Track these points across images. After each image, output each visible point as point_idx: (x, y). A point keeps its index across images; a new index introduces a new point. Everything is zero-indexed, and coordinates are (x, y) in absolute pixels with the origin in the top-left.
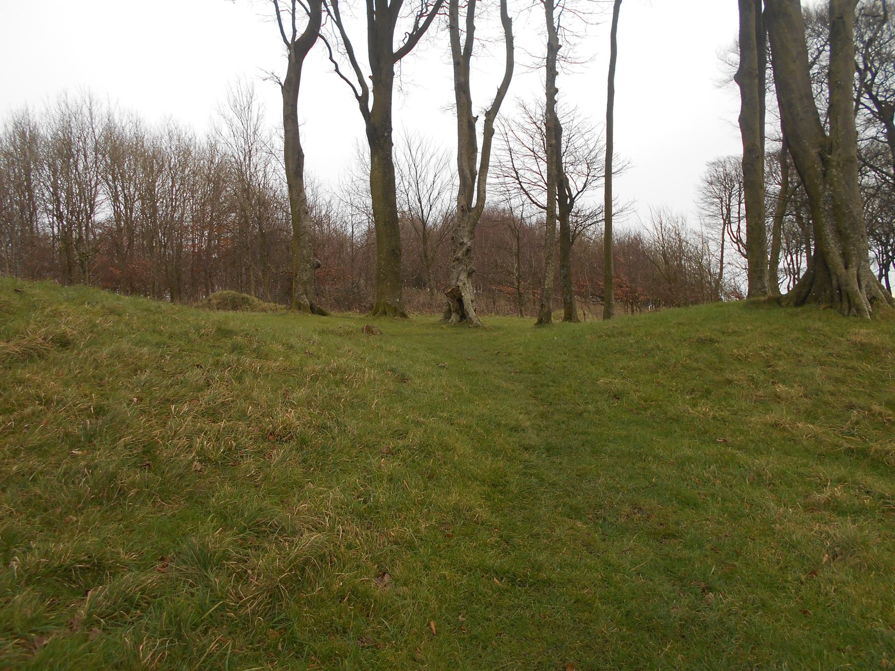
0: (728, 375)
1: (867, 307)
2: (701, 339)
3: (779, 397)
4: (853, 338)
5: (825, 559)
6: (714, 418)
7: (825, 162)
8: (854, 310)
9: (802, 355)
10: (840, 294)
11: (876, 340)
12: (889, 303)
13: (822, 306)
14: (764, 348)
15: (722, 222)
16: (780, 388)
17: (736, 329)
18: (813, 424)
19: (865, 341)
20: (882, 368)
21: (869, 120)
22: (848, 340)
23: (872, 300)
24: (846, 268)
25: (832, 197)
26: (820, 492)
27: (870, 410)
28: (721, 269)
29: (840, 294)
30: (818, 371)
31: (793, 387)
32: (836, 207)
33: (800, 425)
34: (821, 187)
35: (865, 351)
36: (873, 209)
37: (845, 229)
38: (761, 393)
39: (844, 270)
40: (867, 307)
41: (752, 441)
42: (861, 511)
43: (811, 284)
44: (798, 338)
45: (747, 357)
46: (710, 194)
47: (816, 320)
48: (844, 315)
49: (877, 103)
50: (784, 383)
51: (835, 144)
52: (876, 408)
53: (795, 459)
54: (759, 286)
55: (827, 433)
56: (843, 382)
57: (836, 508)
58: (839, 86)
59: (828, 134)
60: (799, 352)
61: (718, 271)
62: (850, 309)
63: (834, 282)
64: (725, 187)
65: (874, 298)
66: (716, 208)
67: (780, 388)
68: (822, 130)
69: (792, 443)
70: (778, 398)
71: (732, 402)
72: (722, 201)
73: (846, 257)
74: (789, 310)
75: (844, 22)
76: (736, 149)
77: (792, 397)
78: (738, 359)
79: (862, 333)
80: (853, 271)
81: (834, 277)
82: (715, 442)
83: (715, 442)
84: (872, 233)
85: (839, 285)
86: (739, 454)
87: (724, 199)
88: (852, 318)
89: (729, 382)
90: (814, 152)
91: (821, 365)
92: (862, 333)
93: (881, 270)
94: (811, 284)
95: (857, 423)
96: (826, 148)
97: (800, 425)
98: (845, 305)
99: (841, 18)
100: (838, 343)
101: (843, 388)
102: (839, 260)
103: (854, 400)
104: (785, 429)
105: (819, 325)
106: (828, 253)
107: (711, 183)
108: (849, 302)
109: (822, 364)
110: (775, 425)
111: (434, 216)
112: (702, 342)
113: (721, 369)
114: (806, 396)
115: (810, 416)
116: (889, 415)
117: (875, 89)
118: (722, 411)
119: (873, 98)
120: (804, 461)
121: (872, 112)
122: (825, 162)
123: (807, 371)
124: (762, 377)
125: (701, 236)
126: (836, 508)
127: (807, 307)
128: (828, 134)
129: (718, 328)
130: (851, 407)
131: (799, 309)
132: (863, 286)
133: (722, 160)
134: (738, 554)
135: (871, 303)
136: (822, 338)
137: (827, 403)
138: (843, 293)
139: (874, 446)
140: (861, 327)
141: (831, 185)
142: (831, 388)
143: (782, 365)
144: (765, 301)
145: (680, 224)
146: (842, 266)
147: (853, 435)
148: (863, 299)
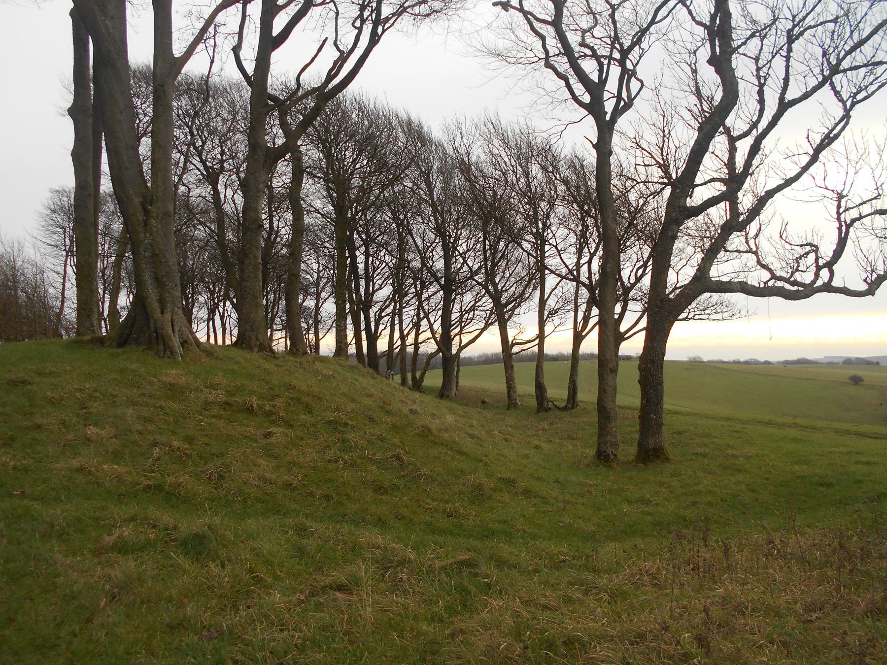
0: (38, 420)
1: (179, 350)
2: (13, 381)
3: (89, 440)
4: (164, 379)
5: (102, 604)
6: (14, 468)
7: (146, 212)
8: (168, 351)
9: (117, 396)
10: (157, 337)
11: (182, 380)
12: (198, 347)
13: (141, 348)
14: (80, 390)
15: (64, 253)
16: (91, 430)
17: (54, 369)
18: (118, 464)
19: (173, 381)
20: (186, 406)
21: (200, 180)
22: (159, 381)
23: (184, 343)
24: (162, 313)
25: (152, 246)
26: (110, 535)
27: (170, 446)
28: (63, 302)
29: (157, 337)
30: (130, 411)
31: (103, 428)
32: (154, 255)
33: (105, 467)
34: (142, 235)
35: (174, 391)
36: (204, 259)
37: (162, 276)
38: (70, 437)
39: (160, 315)
40: (179, 350)
41: (53, 489)
42: (147, 546)
43: (132, 326)
44: (116, 379)
45: (62, 399)
46: (52, 223)
47: (134, 361)
48: (160, 357)
49: (206, 168)
50: (96, 424)
51: (155, 197)
52: (176, 443)
53: (95, 503)
54: (88, 324)
55: (130, 473)
56: (151, 421)
57: (123, 548)
58: (160, 146)
59: (149, 185)
60: (115, 393)
61: (58, 303)
62: (165, 351)
63: (152, 325)
64: (69, 218)
65: (185, 342)
66: (58, 238)
67: (91, 430)
68: (145, 182)
69: (96, 486)
70: (88, 441)
71: (39, 448)
72: (65, 232)
73: (162, 301)
74: (111, 351)
75: (164, 90)
76: (68, 181)
77: (102, 439)
78: (51, 402)
79: (173, 374)
80: (168, 316)
81: (151, 320)
82: (11, 495)
83: (11, 495)
84: (202, 280)
85: (156, 328)
86: (36, 506)
87: (68, 230)
88: (166, 360)
89: (38, 427)
90: (137, 201)
91: (134, 405)
92: (173, 374)
93: (209, 314)
94: (132, 326)
95: (158, 459)
96: (148, 199)
97: (105, 467)
98: (161, 347)
99: (162, 86)
100: (151, 383)
101: (151, 427)
102: (156, 305)
103: (158, 438)
104: (90, 473)
105: (135, 366)
106: (147, 298)
107: (54, 211)
108: (164, 345)
109: (134, 404)
110: (80, 470)
111: (588, 102)
112: (14, 383)
113: (32, 413)
114: (116, 437)
115: (117, 457)
116: (186, 449)
117: (204, 154)
118: (25, 459)
119: (203, 162)
120: (104, 503)
121: (202, 174)
122: (146, 212)
123: (119, 412)
124: (75, 420)
125: (35, 265)
126: (123, 548)
127: (127, 348)
128: (149, 185)
129: (34, 368)
130: (155, 444)
131: (120, 350)
132: (176, 331)
133: (67, 190)
134: (11, 620)
135: (183, 347)
136: (138, 378)
137: (134, 443)
138: (159, 336)
139: (170, 480)
140: (172, 368)
141: (151, 235)
142: (140, 427)
143: (96, 407)
144: (88, 341)
145: (16, 249)
146: (158, 310)
147: (154, 472)
148: (176, 342)
